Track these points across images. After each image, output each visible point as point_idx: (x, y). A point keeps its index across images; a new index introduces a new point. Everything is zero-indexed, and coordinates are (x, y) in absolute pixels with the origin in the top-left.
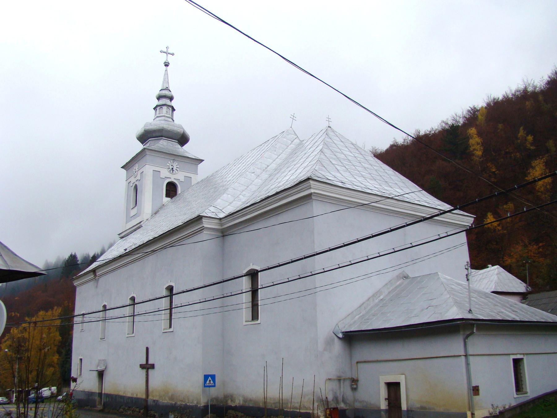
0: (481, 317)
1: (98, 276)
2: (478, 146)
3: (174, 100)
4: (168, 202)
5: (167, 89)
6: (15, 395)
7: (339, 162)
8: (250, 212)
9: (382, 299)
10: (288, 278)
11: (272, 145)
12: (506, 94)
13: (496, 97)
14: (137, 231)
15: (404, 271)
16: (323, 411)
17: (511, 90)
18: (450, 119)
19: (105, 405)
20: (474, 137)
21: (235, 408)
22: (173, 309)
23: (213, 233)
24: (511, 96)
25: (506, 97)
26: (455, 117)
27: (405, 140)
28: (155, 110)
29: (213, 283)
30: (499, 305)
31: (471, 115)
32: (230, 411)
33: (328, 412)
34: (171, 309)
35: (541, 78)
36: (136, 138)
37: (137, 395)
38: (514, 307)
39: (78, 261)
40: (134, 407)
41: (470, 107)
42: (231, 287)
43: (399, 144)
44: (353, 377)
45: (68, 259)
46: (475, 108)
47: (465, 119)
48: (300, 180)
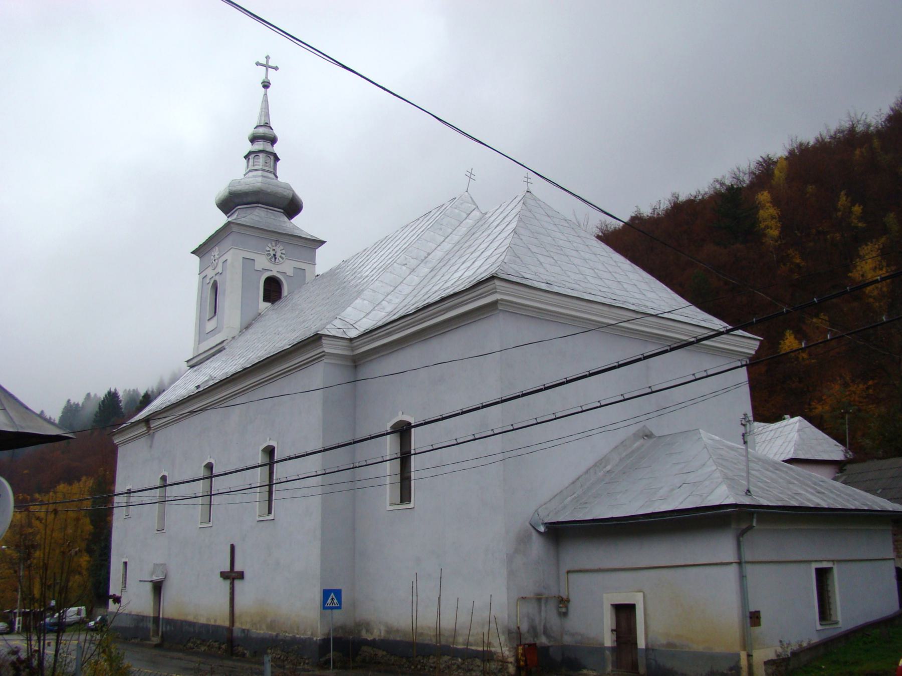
0: (765, 502)
1: (152, 429)
2: (772, 222)
3: (278, 142)
4: (266, 310)
5: (267, 125)
6: (17, 619)
7: (544, 249)
8: (400, 328)
9: (609, 471)
10: (456, 439)
11: (437, 219)
12: (821, 137)
13: (803, 141)
14: (217, 356)
15: (645, 426)
16: (512, 649)
17: (828, 130)
18: (728, 176)
19: (164, 637)
20: (766, 207)
21: (373, 643)
22: (274, 485)
23: (340, 362)
24: (829, 140)
25: (820, 139)
26: (737, 172)
27: (654, 210)
28: (247, 159)
29: (337, 445)
30: (796, 482)
31: (763, 169)
32: (364, 648)
33: (520, 651)
34: (270, 486)
35: (878, 110)
36: (216, 206)
37: (215, 621)
38: (820, 485)
39: (121, 401)
40: (211, 641)
41: (762, 157)
42: (366, 452)
43: (644, 217)
44: (561, 595)
45: (104, 398)
46: (770, 159)
47: (754, 176)
48: (479, 278)
